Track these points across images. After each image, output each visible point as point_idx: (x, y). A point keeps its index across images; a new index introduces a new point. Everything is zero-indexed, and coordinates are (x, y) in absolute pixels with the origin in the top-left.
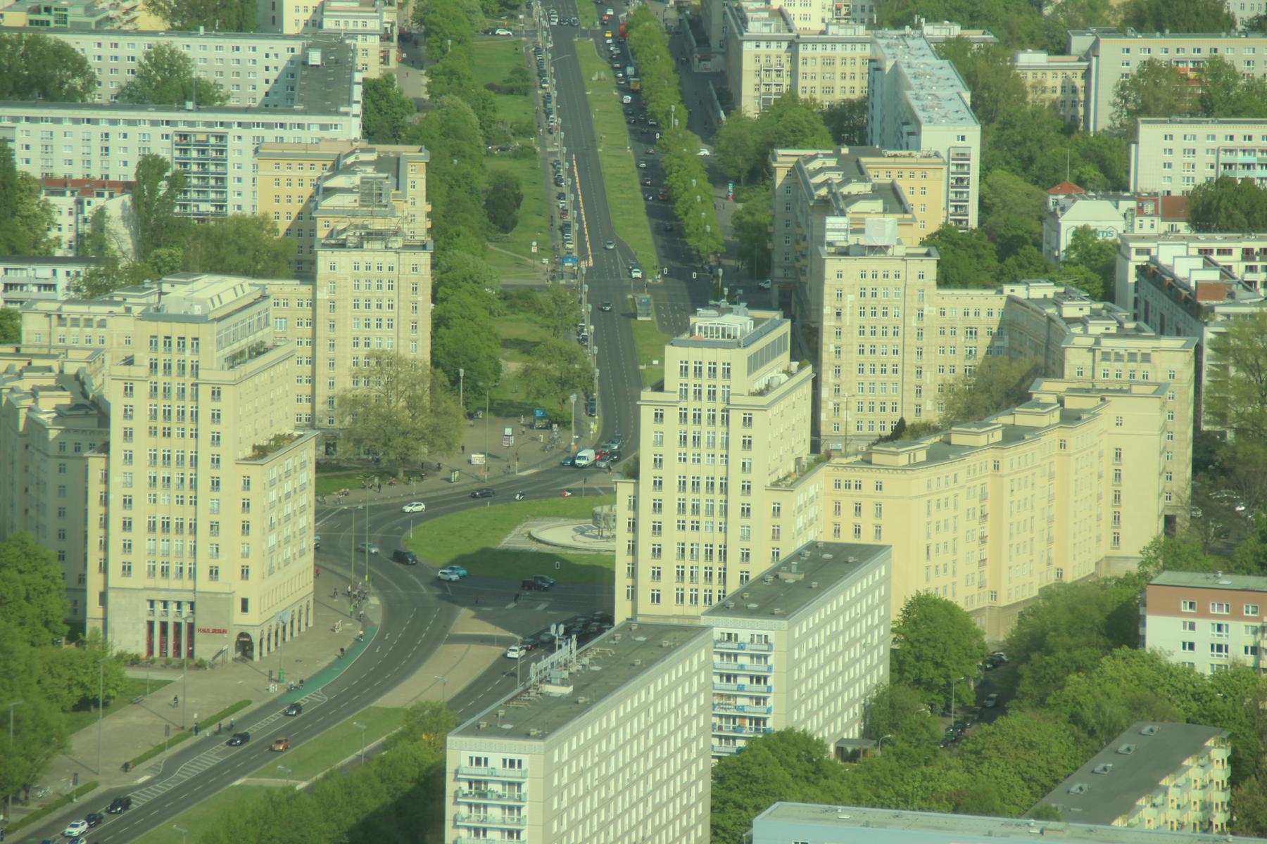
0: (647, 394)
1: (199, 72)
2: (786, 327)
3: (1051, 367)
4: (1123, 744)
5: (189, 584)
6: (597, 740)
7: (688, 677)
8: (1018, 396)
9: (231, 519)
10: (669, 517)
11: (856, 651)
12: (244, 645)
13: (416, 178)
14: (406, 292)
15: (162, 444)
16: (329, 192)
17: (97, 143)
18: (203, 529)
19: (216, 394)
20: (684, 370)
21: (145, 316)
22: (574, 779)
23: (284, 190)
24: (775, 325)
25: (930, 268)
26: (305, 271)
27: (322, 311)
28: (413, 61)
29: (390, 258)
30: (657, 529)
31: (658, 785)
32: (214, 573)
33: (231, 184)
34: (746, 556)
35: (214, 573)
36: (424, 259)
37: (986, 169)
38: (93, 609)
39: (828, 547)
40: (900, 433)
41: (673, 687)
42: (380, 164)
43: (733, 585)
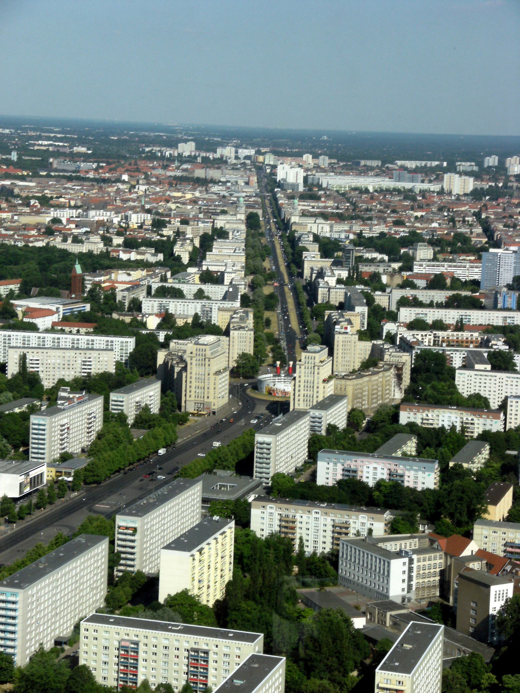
2: (327, 349)
7: (305, 422)
8: (375, 365)
10: (302, 388)
13: (251, 316)
14: (248, 340)
15: (306, 392)
16: (233, 318)
18: (206, 388)
20: (306, 358)
26: (227, 333)
27: (231, 343)
29: (245, 332)
30: (299, 391)
31: (299, 445)
32: (208, 397)
34: (317, 397)
37: (369, 317)
38: (183, 404)
39: (335, 395)
40: (354, 372)
42: (243, 312)
43: (315, 403)
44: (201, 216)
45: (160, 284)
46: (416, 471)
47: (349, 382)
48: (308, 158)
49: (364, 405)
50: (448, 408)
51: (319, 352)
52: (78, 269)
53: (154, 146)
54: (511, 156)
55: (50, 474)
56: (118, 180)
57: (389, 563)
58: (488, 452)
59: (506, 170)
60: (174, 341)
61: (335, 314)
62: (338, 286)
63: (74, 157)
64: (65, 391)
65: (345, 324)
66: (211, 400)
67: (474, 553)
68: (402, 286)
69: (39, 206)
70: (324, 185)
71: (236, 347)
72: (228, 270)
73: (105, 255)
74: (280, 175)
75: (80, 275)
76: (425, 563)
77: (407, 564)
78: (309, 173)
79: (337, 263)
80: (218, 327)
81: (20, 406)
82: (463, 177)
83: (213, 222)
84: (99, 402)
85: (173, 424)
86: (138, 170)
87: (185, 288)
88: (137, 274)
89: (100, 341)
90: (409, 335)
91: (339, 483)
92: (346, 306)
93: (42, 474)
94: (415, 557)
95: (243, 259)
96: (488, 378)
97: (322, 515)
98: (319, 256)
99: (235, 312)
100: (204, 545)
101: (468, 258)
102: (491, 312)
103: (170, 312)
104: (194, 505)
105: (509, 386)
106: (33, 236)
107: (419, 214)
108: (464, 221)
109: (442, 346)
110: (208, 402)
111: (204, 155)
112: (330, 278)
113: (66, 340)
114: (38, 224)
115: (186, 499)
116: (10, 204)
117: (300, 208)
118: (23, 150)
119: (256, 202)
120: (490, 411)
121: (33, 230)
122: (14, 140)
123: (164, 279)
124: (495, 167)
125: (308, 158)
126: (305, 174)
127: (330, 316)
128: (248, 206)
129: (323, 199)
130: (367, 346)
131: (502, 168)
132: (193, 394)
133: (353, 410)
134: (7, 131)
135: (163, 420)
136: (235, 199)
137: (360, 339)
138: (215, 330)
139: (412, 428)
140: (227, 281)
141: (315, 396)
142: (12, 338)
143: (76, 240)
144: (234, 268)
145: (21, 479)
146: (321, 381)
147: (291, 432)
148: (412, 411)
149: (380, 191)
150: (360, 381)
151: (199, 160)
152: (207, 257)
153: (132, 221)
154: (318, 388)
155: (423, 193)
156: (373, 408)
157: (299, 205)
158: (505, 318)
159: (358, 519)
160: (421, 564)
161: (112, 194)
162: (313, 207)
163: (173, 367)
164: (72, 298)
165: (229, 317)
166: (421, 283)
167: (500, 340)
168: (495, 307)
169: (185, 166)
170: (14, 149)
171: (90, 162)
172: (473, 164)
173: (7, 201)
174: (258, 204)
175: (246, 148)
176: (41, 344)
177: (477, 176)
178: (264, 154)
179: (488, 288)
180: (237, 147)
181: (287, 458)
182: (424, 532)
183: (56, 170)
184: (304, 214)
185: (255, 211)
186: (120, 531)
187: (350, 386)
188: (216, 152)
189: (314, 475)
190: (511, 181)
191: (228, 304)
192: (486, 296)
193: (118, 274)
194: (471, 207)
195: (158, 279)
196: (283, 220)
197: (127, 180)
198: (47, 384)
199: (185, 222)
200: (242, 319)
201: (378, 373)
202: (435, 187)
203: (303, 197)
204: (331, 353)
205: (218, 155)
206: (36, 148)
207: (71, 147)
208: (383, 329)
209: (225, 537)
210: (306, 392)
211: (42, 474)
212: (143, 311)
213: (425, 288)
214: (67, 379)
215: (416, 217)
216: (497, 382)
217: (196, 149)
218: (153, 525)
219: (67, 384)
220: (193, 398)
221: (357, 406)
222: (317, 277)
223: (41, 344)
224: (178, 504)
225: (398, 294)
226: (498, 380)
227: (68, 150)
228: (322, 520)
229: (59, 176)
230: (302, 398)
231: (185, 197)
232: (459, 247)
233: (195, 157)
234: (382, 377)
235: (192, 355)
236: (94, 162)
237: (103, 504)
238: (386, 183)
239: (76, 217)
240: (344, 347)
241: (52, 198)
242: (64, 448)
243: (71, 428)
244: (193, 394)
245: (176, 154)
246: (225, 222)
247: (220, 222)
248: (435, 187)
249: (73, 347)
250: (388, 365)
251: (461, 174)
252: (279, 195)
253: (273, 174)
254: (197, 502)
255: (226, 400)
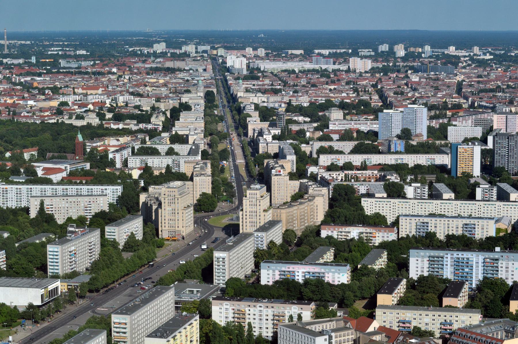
0: (244, 198)
1: (176, 151)
2: (265, 187)
3: (307, 193)
4: (318, 250)
5: (174, 228)
6: (237, 251)
7: (251, 241)
8: (302, 197)
9: (181, 219)
10: (248, 217)
11: (277, 237)
12: (183, 238)
13: (209, 165)
14: (207, 183)
15: (251, 220)
16: (195, 168)
17: (160, 161)
18: (176, 220)
19: (178, 199)
20: (250, 194)
21: (167, 188)
22: (233, 257)
23: (189, 168)
24: (263, 187)
25: (288, 177)
26: (191, 179)
27: (194, 186)
28: (210, 148)
29: (205, 178)
30: (246, 219)
31: (247, 258)
32: (178, 227)
33: (181, 167)
34: (260, 223)
35: (178, 227)
36: (210, 178)
37: (297, 163)
38: (160, 233)
39: (272, 221)
40: (285, 204)
41: (248, 243)
42: (203, 163)
43: (258, 227)
44: (171, 95)
45: (140, 146)
46: (333, 273)
47: (282, 211)
48: (249, 51)
49: (295, 227)
50: (356, 226)
51: (260, 189)
52: (80, 137)
53: (135, 47)
54: (398, 44)
55: (63, 288)
56: (110, 73)
57: (314, 340)
58: (386, 257)
59: (394, 53)
60: (152, 186)
61: (272, 162)
62: (273, 141)
63: (78, 58)
64: (72, 226)
65: (279, 169)
66: (181, 228)
67: (376, 329)
68: (320, 139)
69: (52, 94)
70: (262, 69)
71: (198, 189)
72: (191, 133)
73: (101, 126)
74: (229, 64)
75: (81, 142)
76: (341, 338)
77: (328, 340)
78: (251, 61)
79: (273, 125)
80: (185, 174)
81: (40, 239)
82: (364, 60)
83: (180, 99)
84: (98, 233)
85: (153, 247)
86: (124, 65)
87: (159, 147)
88: (123, 140)
89: (97, 189)
90: (327, 175)
91: (276, 282)
92: (280, 155)
93: (57, 288)
94: (333, 334)
95: (203, 125)
96: (509, 207)
97: (264, 308)
98: (259, 120)
99: (197, 164)
100: (177, 333)
101: (369, 117)
102: (386, 156)
103: (149, 165)
104: (169, 306)
105: (400, 209)
106: (48, 116)
107: (332, 87)
108: (365, 91)
109: (351, 182)
110: (178, 230)
111: (173, 51)
112: (268, 136)
113: (72, 189)
114: (51, 107)
115: (163, 301)
116: (30, 94)
117: (244, 86)
118: (40, 55)
119: (212, 84)
120: (387, 226)
121: (47, 111)
122: (34, 48)
123: (144, 142)
124: (386, 52)
125: (249, 51)
126: (248, 62)
127: (268, 164)
128: (205, 87)
129: (261, 79)
130: (296, 185)
131: (391, 53)
132: (167, 225)
133: (287, 231)
134: (28, 42)
135: (145, 244)
136: (196, 82)
137: (291, 179)
138: (182, 177)
139: (330, 241)
140: (191, 141)
141: (258, 222)
142: (33, 190)
143: (80, 117)
144: (196, 132)
145: (42, 291)
146: (262, 211)
147: (240, 249)
148: (330, 230)
149: (304, 72)
150: (291, 209)
151: (169, 55)
152: (176, 124)
153: (120, 101)
154: (260, 216)
155: (334, 71)
156: (302, 229)
157: (243, 84)
158: (396, 160)
159: (291, 309)
160: (338, 339)
161: (105, 83)
162: (254, 85)
163: (151, 205)
164: (76, 159)
165: (192, 168)
166: (335, 137)
167: (393, 176)
168: (389, 152)
169: (158, 60)
170: (34, 55)
171: (89, 61)
172: (371, 50)
173: (28, 91)
174: (213, 85)
175: (204, 45)
176: (54, 193)
177: (374, 59)
178: (216, 49)
179: (384, 139)
180: (197, 44)
181: (238, 268)
182: (340, 316)
183: (64, 68)
184: (247, 90)
185: (210, 89)
186: (115, 326)
187: (284, 214)
188: (181, 49)
189: (258, 279)
190: (398, 62)
191: (191, 158)
192: (382, 144)
193: (110, 140)
194: (370, 81)
195: (139, 143)
196: (232, 95)
197: (115, 72)
198: (60, 221)
199: (158, 100)
200: (202, 168)
201: (304, 203)
202: (344, 67)
203: (246, 78)
204: (269, 190)
205: (183, 51)
206: (49, 53)
207: (74, 51)
208: (308, 171)
209: (193, 327)
210: (251, 220)
211: (57, 288)
212: (129, 166)
213: (337, 140)
214: (74, 217)
215: (330, 90)
216: (391, 206)
217: (166, 48)
218: (139, 321)
219: (74, 221)
220: (167, 228)
221: (290, 228)
222: (257, 136)
223: (54, 193)
224: (157, 305)
225: (317, 145)
226: (392, 205)
227: (72, 53)
228: (265, 311)
229: (66, 72)
230: (248, 224)
231: (159, 82)
232: (363, 110)
233: (166, 53)
234: (307, 206)
235: (165, 196)
236: (91, 61)
237: (103, 308)
238: (308, 66)
239: (79, 101)
240: (279, 186)
241: (61, 88)
242: (73, 268)
243: (77, 253)
244: (167, 225)
245: (152, 52)
246: (188, 98)
247: (185, 99)
248: (344, 67)
249: (77, 194)
250: (312, 197)
251: (362, 57)
252: (228, 78)
253: (224, 62)
254: (172, 303)
255: (192, 228)
